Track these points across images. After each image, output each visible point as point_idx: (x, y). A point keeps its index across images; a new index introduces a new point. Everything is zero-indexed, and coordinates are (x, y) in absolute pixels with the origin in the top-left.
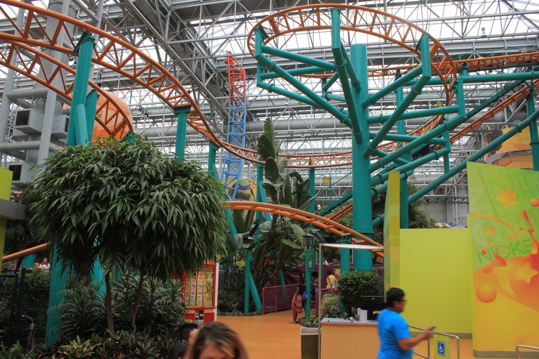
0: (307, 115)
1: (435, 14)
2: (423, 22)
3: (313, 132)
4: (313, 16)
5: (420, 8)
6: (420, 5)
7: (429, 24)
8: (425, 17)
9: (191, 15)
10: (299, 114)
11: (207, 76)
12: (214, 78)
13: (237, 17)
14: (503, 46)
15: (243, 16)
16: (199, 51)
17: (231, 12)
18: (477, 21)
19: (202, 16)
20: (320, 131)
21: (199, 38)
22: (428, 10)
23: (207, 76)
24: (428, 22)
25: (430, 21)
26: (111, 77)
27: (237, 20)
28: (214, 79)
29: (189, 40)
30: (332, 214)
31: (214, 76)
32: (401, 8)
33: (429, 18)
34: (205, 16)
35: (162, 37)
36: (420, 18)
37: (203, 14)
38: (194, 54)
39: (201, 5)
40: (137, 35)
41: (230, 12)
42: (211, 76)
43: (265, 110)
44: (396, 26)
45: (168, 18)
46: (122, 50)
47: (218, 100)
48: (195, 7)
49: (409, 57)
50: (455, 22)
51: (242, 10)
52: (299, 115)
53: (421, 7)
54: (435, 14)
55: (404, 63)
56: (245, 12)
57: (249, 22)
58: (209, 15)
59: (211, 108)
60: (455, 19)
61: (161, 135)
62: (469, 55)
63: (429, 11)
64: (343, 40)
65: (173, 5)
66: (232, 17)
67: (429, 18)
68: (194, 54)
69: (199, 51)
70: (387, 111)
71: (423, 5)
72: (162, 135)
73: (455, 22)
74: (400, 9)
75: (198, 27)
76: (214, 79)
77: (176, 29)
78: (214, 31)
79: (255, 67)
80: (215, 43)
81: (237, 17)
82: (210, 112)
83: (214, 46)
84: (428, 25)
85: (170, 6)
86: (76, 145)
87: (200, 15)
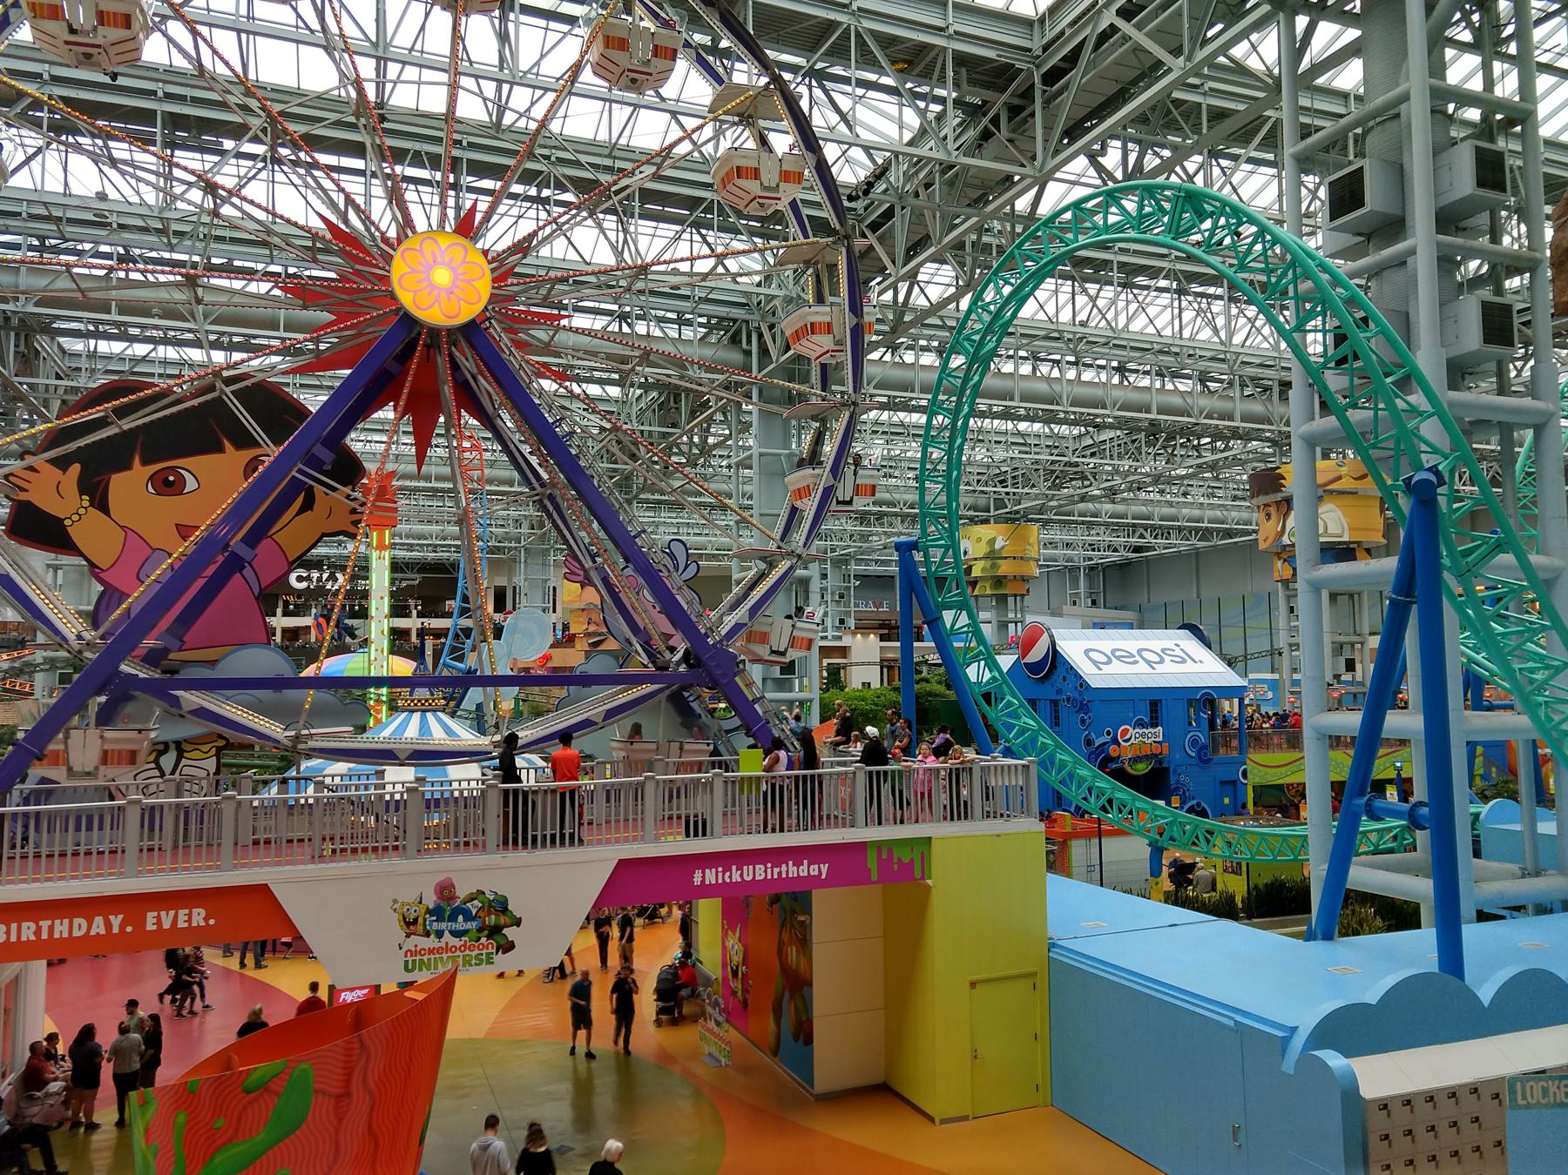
14: (940, 23)
70: (662, 225)
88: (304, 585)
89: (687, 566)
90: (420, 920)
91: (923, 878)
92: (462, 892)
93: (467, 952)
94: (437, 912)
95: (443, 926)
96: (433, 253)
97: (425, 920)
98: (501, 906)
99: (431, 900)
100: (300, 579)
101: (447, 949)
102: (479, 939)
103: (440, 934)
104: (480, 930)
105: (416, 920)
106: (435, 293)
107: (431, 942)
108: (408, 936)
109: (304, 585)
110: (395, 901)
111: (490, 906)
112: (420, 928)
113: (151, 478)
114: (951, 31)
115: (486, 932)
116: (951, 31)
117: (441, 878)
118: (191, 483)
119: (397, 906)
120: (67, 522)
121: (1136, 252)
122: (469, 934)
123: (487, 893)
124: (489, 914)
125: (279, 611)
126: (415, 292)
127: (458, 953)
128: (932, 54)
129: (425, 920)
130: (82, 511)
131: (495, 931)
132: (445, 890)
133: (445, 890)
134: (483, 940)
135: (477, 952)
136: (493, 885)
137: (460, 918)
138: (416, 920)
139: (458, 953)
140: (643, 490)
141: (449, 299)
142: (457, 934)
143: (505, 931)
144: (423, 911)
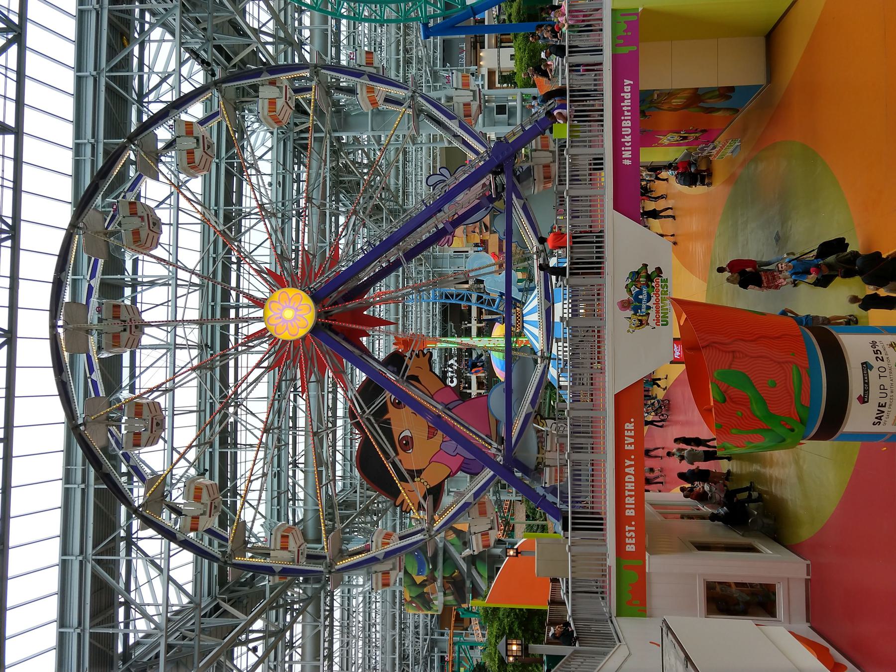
0: (239, 461)
1: (256, 249)
10: (234, 477)
11: (225, 613)
12: (229, 601)
13: (123, 553)
15: (123, 544)
16: (178, 634)
17: (111, 566)
19: (113, 627)
23: (225, 613)
27: (128, 553)
28: (231, 602)
29: (162, 649)
30: (490, 441)
31: (225, 602)
34: (112, 620)
37: (106, 625)
38: (182, 642)
41: (112, 568)
42: (227, 606)
47: (271, 593)
48: (90, 644)
51: (112, 545)
52: (238, 476)
54: (256, 249)
56: (117, 540)
57: (136, 532)
58: (112, 611)
59: (272, 608)
62: (227, 170)
64: (183, 368)
68: (182, 642)
69: (178, 634)
75: (132, 635)
76: (231, 602)
78: (151, 601)
80: (173, 599)
81: (123, 553)
82: (281, 610)
83: (177, 600)
87: (111, 631)
88: (455, 380)
89: (442, 175)
90: (640, 318)
91: (637, 14)
92: (626, 296)
93: (660, 293)
94: (636, 310)
95: (644, 306)
96: (276, 319)
97: (640, 316)
98: (635, 275)
99: (629, 313)
100: (452, 382)
101: (657, 304)
102: (653, 287)
103: (649, 308)
104: (648, 286)
105: (640, 320)
106: (298, 317)
107: (652, 312)
108: (648, 324)
109: (455, 380)
110: (628, 331)
111: (635, 281)
112: (644, 318)
113: (405, 451)
114: (97, 6)
115: (649, 283)
116: (97, 6)
117: (617, 308)
118: (407, 433)
119: (631, 331)
120: (428, 487)
121: (420, 390)
122: (650, 292)
123: (627, 283)
124: (639, 281)
125: (468, 391)
126: (299, 328)
127: (660, 298)
128: (113, 18)
129: (640, 316)
130: (422, 481)
131: (649, 278)
132: (624, 305)
133: (624, 305)
134: (654, 284)
135: (660, 288)
136: (623, 279)
137: (640, 297)
138: (640, 320)
139: (660, 298)
140: (397, 202)
141: (300, 310)
142: (649, 298)
143: (649, 273)
144: (635, 317)
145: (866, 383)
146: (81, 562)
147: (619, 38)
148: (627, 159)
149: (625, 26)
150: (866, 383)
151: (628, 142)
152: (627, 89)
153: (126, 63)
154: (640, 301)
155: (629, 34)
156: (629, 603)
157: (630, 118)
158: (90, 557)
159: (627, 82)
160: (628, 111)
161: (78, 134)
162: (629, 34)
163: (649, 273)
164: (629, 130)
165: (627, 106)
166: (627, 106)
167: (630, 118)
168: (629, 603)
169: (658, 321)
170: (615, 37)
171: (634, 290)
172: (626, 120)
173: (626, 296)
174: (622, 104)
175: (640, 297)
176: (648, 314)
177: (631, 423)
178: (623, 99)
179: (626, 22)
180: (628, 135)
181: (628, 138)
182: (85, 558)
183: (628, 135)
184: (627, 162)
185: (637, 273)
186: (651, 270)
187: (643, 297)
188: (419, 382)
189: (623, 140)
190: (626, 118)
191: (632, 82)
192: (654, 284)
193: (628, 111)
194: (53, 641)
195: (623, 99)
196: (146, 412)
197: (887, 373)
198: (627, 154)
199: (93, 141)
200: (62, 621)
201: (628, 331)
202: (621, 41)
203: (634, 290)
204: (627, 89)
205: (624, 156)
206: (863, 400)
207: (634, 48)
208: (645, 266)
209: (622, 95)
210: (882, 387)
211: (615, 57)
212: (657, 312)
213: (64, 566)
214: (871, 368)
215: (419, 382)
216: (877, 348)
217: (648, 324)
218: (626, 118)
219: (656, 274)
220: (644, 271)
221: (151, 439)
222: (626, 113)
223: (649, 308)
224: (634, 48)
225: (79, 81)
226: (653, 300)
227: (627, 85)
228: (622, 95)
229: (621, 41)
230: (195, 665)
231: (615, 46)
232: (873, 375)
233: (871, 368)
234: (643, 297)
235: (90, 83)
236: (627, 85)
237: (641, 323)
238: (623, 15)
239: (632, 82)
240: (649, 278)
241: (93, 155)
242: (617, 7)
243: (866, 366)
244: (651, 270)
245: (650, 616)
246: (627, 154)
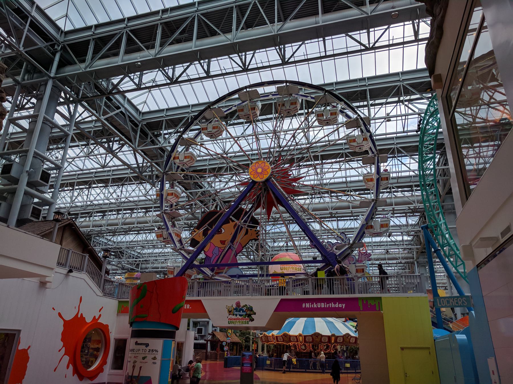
2: (401, 116)
3: (331, 213)
4: (400, 105)
5: (398, 107)
6: (399, 104)
7: (408, 119)
8: (403, 112)
9: (389, 96)
18: (382, 122)
20: (337, 213)
21: (162, 145)
22: (406, 107)
24: (407, 117)
25: (408, 115)
26: (105, 175)
32: (382, 107)
33: (407, 113)
35: (133, 144)
36: (399, 113)
39: (164, 119)
40: (115, 143)
43: (152, 207)
44: (103, 154)
45: (139, 130)
46: (106, 154)
49: (392, 148)
50: (397, 120)
53: (400, 105)
55: (336, 158)
60: (397, 117)
61: (150, 222)
63: (407, 108)
65: (143, 119)
66: (390, 100)
67: (407, 113)
71: (401, 104)
72: (151, 223)
73: (397, 120)
74: (380, 108)
77: (147, 138)
79: (418, 144)
84: (406, 120)
85: (140, 120)
86: (443, 202)
87: (163, 127)
91: (379, 310)
92: (242, 304)
94: (236, 309)
95: (237, 313)
98: (251, 309)
101: (238, 319)
103: (236, 315)
104: (246, 315)
105: (231, 311)
107: (234, 317)
108: (229, 315)
110: (227, 306)
112: (232, 313)
118: (223, 231)
124: (248, 311)
131: (249, 315)
132: (238, 304)
133: (238, 304)
134: (247, 317)
136: (249, 303)
137: (241, 311)
138: (231, 311)
142: (240, 315)
143: (252, 316)
145: (141, 344)
146: (189, 112)
147: (367, 301)
148: (305, 305)
149: (373, 304)
150: (141, 344)
151: (314, 306)
152: (340, 306)
153: (407, 92)
154: (239, 311)
155: (369, 306)
156: (123, 306)
157: (326, 307)
158: (190, 115)
159: (344, 305)
160: (329, 306)
161: (369, 78)
162: (369, 306)
163: (252, 316)
164: (320, 307)
165: (331, 306)
166: (331, 306)
167: (326, 307)
168: (123, 306)
169: (230, 319)
170: (367, 299)
171: (245, 309)
172: (324, 305)
173: (242, 304)
174: (332, 303)
175: (241, 311)
176: (234, 315)
177: (190, 307)
178: (335, 304)
179: (375, 305)
180: (317, 306)
181: (315, 306)
182: (190, 113)
183: (317, 306)
184: (304, 306)
185: (252, 310)
186: (253, 316)
187: (241, 313)
188: (245, 235)
189: (315, 303)
190: (326, 305)
191: (344, 308)
192: (247, 317)
193: (329, 306)
194: (162, 108)
195: (335, 304)
196: (333, 117)
197: (144, 352)
198: (308, 305)
199: (367, 85)
200: (168, 110)
201: (227, 306)
202: (365, 302)
203: (245, 309)
204: (340, 306)
205: (307, 304)
206: (137, 343)
207: (361, 309)
208: (255, 314)
209: (337, 303)
210: (139, 350)
211: (357, 299)
212: (234, 319)
213: (188, 106)
214: (146, 347)
215: (245, 235)
216: (154, 352)
217: (229, 315)
218: (326, 305)
219: (251, 319)
220: (253, 313)
221: (321, 121)
222: (328, 305)
223: (236, 315)
224: (361, 309)
225: (397, 74)
226: (240, 317)
227: (342, 305)
228: (337, 303)
229: (365, 302)
230: (153, 161)
231: (363, 299)
232: (144, 347)
233: (146, 347)
234: (241, 313)
235: (398, 79)
236: (342, 305)
237: (230, 312)
238: (379, 303)
239: (344, 308)
240: (249, 315)
241: (360, 86)
242: (383, 300)
243: (147, 345)
244: (253, 316)
245: (117, 315)
246: (308, 305)
